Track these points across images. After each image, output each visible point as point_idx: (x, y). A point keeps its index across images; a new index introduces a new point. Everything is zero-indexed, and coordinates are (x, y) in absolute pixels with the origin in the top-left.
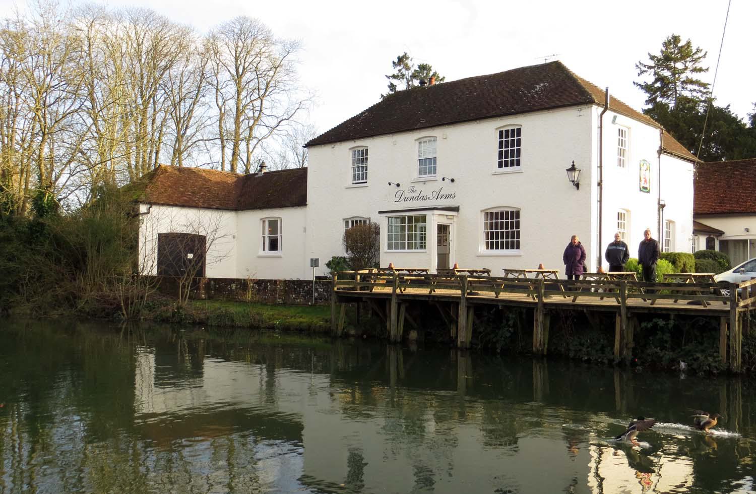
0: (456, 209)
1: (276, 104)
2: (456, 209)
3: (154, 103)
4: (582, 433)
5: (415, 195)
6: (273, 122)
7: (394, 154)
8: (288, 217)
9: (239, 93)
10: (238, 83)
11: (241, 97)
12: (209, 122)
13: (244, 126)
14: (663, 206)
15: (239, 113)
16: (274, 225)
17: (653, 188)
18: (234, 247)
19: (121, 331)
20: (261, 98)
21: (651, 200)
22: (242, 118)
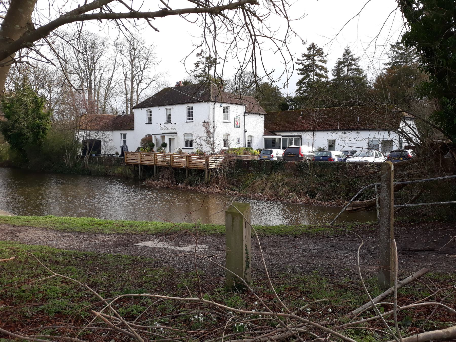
0: (176, 133)
1: (150, 73)
2: (176, 133)
3: (95, 72)
4: (247, 204)
5: (165, 128)
6: (148, 81)
7: (159, 113)
8: (129, 134)
9: (133, 68)
10: (132, 65)
11: (134, 70)
12: (120, 82)
13: (135, 83)
14: (246, 131)
15: (133, 77)
16: (125, 136)
17: (241, 125)
18: (112, 142)
19: (394, 188)
20: (142, 71)
21: (241, 130)
22: (134, 80)
